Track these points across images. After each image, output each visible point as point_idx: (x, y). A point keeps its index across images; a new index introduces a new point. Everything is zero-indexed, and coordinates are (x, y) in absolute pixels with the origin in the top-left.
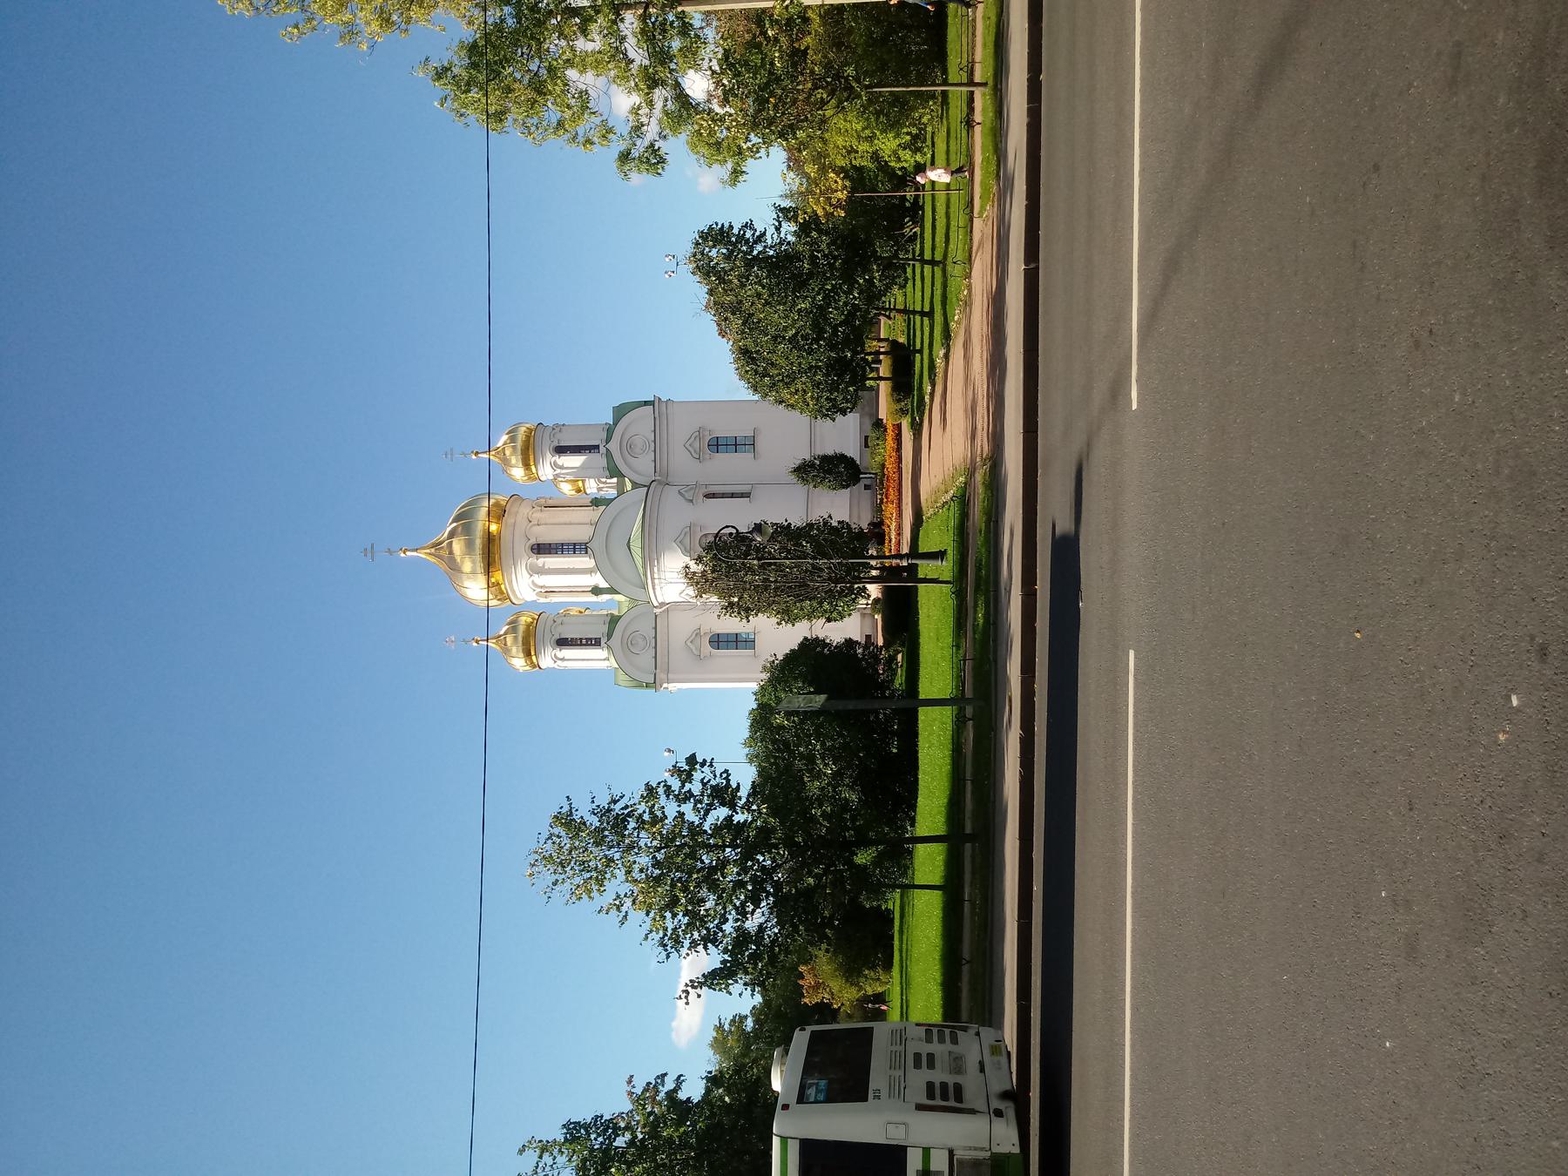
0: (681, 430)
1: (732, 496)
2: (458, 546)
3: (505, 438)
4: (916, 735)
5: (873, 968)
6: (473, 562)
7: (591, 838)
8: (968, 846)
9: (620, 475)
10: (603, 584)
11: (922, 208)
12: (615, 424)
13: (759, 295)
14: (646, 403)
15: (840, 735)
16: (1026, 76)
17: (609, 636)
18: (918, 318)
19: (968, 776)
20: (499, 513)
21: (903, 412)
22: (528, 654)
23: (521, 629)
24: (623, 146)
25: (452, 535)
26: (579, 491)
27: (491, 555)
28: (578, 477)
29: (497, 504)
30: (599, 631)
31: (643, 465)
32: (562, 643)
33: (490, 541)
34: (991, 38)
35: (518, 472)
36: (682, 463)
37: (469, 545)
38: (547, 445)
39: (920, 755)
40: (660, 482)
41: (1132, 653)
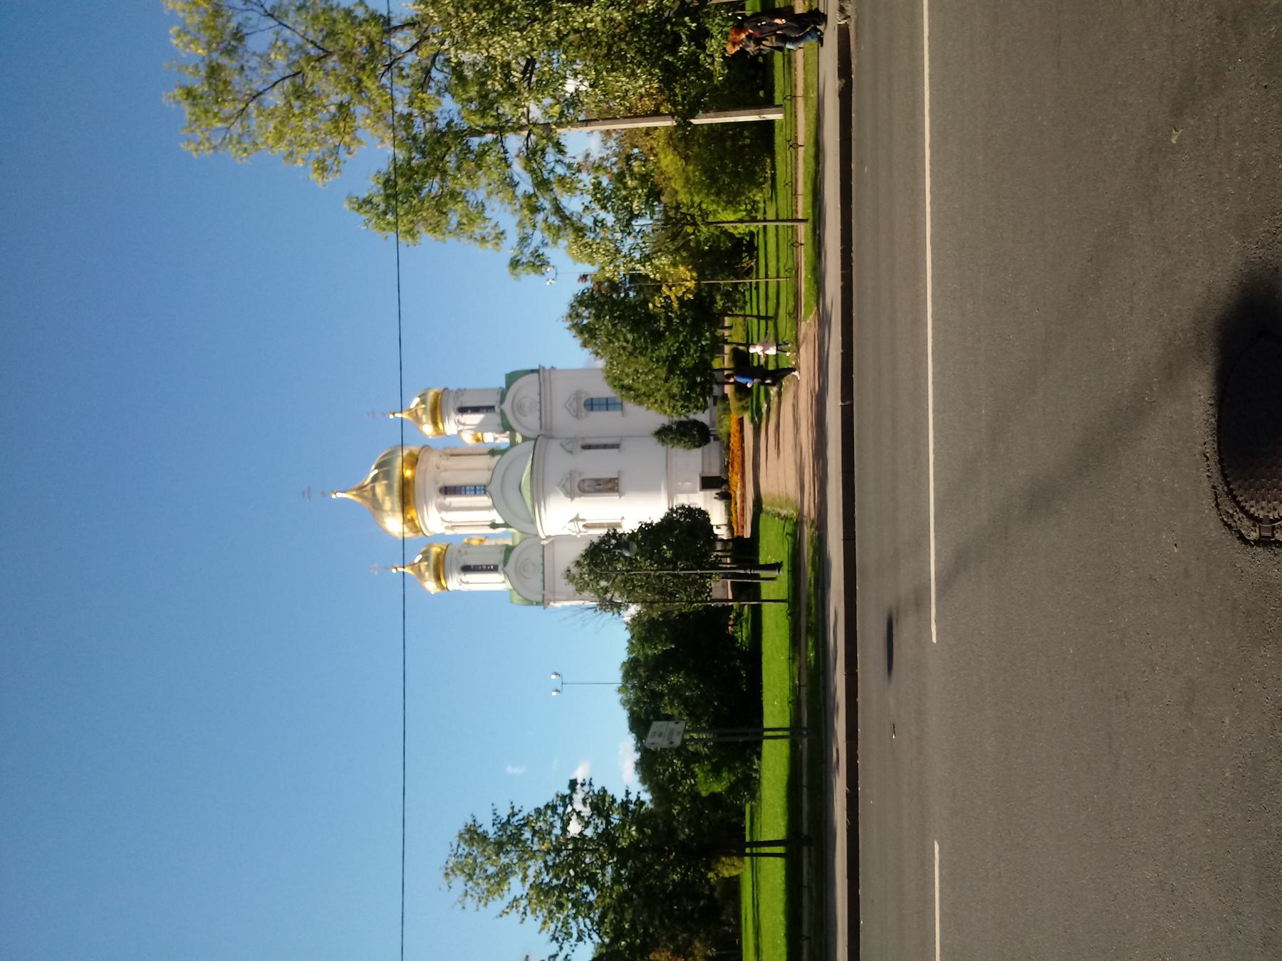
0: (561, 394)
1: (605, 447)
2: (380, 489)
3: (417, 400)
4: (761, 687)
5: (729, 855)
6: (393, 502)
7: (494, 846)
8: (805, 849)
9: (513, 431)
10: (500, 521)
11: (757, 249)
12: (508, 386)
13: (624, 348)
14: (533, 371)
15: (697, 687)
16: (840, 351)
17: (505, 562)
18: (755, 321)
19: (805, 780)
20: (413, 461)
21: (744, 408)
22: (438, 579)
23: (432, 558)
24: (511, 253)
25: (375, 479)
26: (478, 440)
27: (407, 496)
28: (482, 428)
29: (411, 454)
30: (497, 558)
31: (531, 422)
32: (467, 569)
33: (406, 485)
34: (810, 186)
35: (428, 429)
36: (563, 419)
37: (389, 488)
38: (452, 405)
39: (764, 703)
40: (545, 436)
41: (934, 640)
